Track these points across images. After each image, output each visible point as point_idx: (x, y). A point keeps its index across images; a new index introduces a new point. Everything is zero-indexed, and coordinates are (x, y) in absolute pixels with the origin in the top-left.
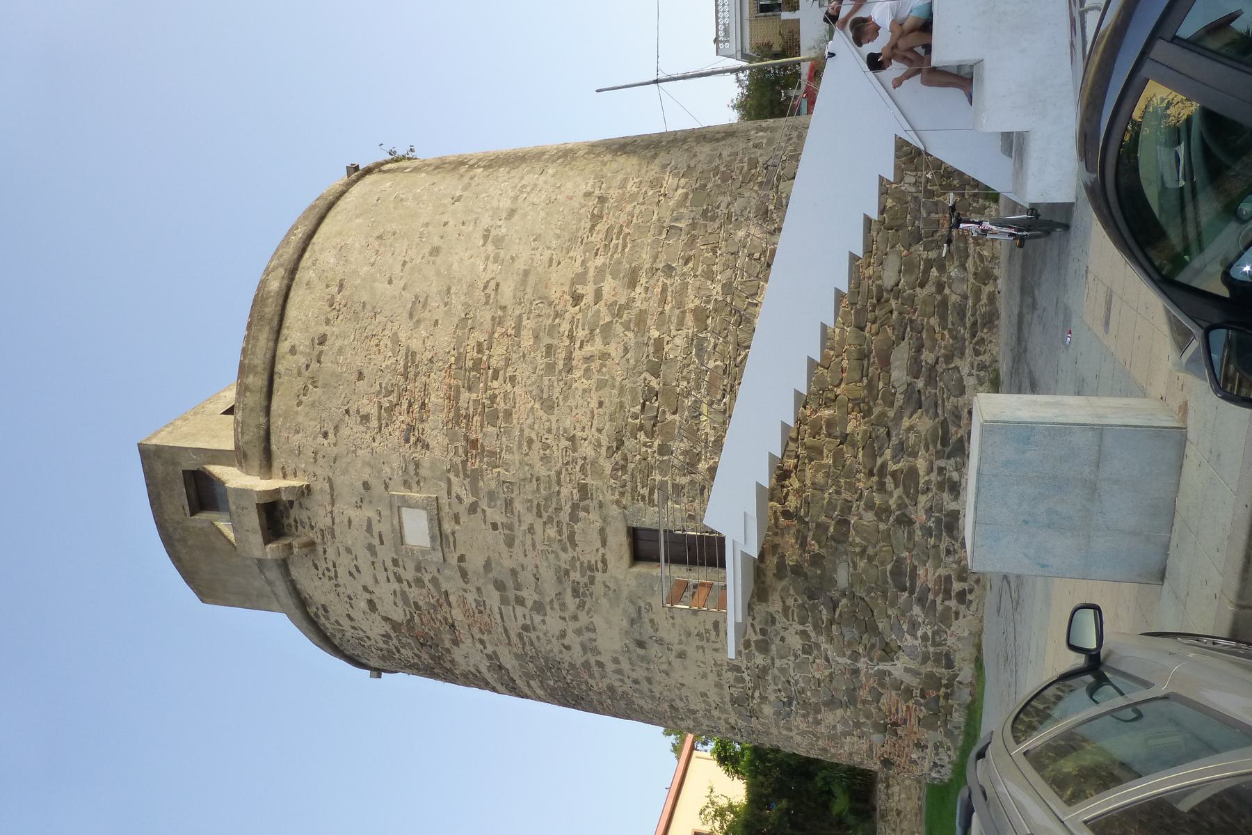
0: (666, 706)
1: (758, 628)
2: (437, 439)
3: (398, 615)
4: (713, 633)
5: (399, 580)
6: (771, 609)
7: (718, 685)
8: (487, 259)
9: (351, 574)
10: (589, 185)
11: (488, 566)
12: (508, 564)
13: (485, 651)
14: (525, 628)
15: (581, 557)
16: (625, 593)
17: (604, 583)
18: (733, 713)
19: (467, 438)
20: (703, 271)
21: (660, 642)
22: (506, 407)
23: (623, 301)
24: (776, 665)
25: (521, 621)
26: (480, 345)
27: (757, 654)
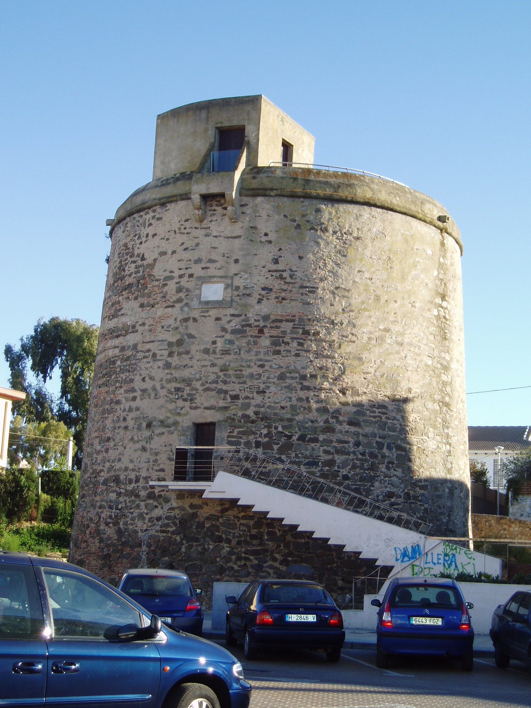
0: (109, 435)
1: (162, 493)
2: (265, 308)
3: (158, 272)
4: (158, 468)
5: (181, 276)
6: (173, 501)
7: (126, 469)
8: (370, 333)
9: (183, 244)
10: (416, 390)
11: (191, 336)
12: (194, 349)
13: (138, 325)
14: (154, 355)
15: (198, 394)
16: (179, 419)
17: (184, 407)
18: (108, 475)
19: (265, 326)
20: (356, 464)
21: (151, 438)
22: (282, 352)
23: (341, 418)
24: (141, 502)
25: (158, 352)
26: (318, 333)
27: (147, 492)
